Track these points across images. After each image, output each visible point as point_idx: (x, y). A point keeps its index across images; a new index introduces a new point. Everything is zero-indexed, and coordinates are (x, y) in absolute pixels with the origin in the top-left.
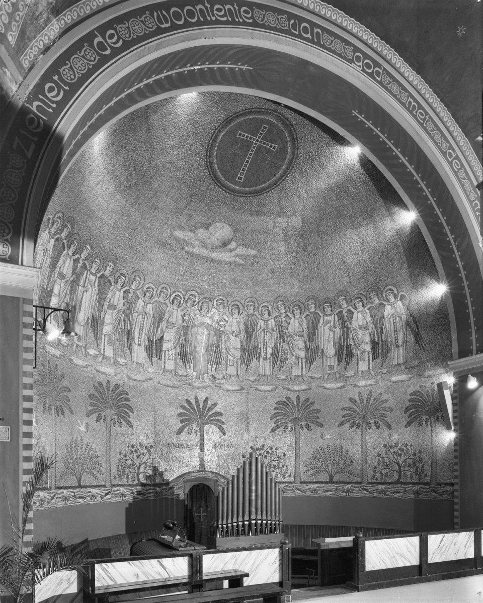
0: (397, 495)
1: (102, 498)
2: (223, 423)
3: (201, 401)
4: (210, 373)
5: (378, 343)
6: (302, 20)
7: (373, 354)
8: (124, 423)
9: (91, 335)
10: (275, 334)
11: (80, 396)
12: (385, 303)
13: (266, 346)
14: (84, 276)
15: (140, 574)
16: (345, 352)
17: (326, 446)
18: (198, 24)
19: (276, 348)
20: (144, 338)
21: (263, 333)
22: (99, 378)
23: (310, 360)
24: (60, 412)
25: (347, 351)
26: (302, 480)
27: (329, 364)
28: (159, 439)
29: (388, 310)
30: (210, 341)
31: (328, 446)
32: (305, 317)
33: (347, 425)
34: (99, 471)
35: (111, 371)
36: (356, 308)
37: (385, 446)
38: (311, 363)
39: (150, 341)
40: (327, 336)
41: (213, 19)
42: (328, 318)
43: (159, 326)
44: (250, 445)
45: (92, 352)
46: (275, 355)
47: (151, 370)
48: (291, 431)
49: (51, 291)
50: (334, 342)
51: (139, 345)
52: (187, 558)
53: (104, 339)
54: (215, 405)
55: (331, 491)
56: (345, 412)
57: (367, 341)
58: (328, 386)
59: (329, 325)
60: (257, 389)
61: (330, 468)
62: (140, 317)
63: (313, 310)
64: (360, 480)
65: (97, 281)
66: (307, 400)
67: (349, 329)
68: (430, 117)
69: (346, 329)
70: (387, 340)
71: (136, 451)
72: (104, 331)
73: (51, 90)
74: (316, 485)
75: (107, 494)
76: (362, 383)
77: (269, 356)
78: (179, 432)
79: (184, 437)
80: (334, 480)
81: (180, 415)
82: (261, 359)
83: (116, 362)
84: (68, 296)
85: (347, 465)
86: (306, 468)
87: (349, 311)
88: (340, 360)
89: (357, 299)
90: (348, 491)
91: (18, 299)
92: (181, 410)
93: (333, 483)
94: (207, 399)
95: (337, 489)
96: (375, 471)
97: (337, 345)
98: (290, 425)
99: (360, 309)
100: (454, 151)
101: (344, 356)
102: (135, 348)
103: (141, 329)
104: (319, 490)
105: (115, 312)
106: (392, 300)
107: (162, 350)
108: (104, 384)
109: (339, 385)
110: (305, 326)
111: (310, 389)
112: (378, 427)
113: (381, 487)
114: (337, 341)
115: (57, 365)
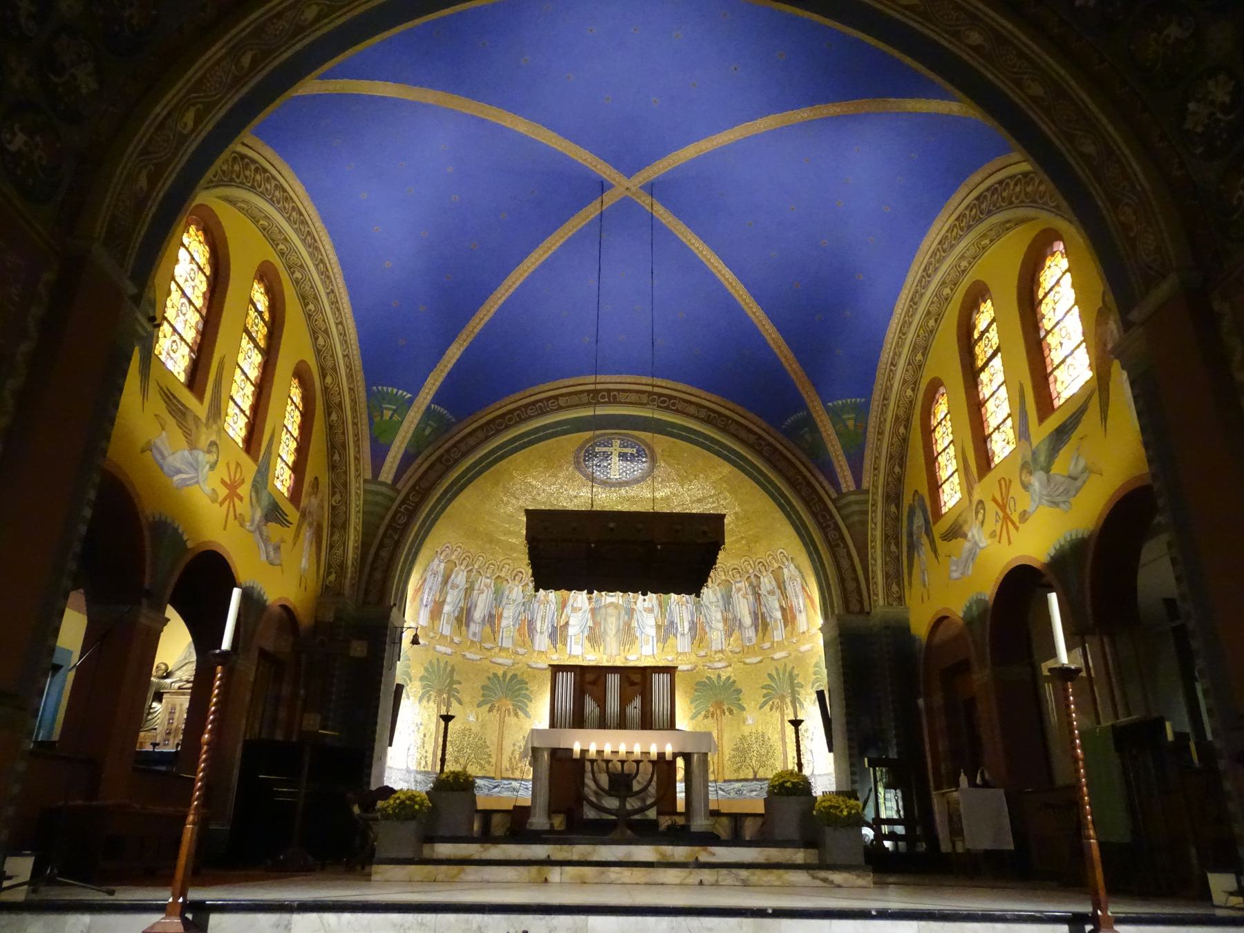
1: (489, 790)
9: (488, 629)
14: (479, 582)
19: (693, 621)
26: (726, 778)
32: (718, 585)
34: (489, 763)
38: (731, 635)
46: (693, 627)
50: (750, 613)
51: (542, 633)
55: (756, 791)
56: (765, 691)
58: (748, 661)
59: (741, 592)
62: (542, 606)
66: (729, 678)
67: (759, 595)
75: (495, 787)
77: (686, 632)
80: (758, 777)
82: (678, 635)
88: (757, 631)
102: (537, 637)
103: (543, 618)
108: (500, 673)
109: (758, 659)
110: (719, 596)
111: (730, 666)
114: (752, 610)
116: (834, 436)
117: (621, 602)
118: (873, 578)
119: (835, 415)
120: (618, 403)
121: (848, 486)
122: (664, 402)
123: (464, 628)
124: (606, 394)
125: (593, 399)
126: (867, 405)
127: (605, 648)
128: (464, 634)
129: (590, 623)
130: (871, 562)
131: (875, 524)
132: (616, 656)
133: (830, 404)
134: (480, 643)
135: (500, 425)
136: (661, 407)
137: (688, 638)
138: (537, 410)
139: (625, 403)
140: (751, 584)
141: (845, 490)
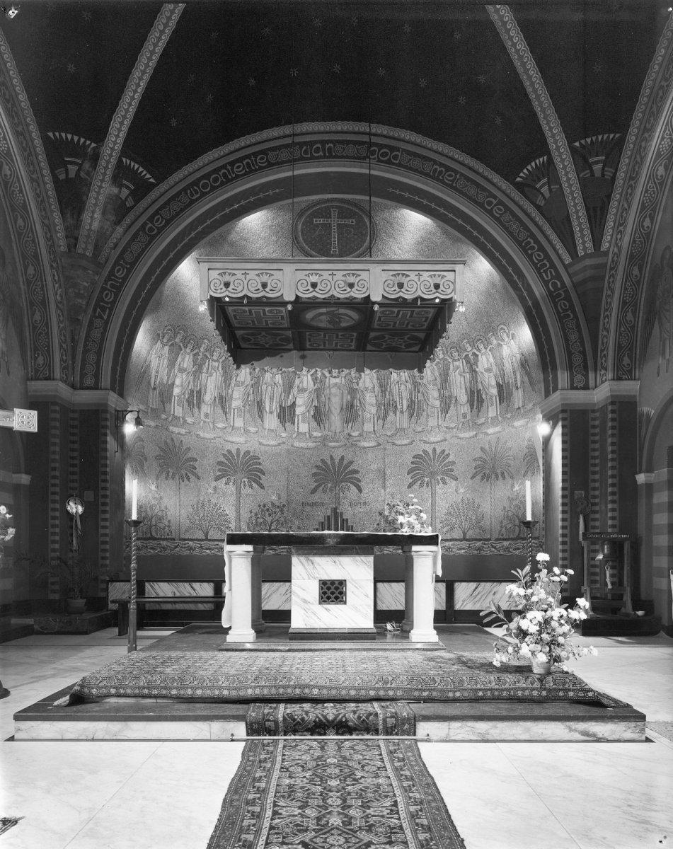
0: (517, 552)
2: (360, 481)
3: (337, 461)
4: (346, 432)
5: (502, 386)
6: (312, 143)
7: (500, 398)
8: (254, 485)
9: (219, 411)
10: (409, 385)
11: (207, 465)
12: (502, 343)
13: (401, 398)
15: (176, 592)
16: (476, 398)
17: (460, 500)
18: (223, 184)
19: (411, 400)
20: (275, 405)
21: (397, 386)
22: (228, 447)
23: (445, 410)
24: (185, 479)
25: (478, 397)
27: (462, 412)
28: (292, 498)
29: (506, 351)
30: (345, 401)
31: (462, 500)
32: (436, 365)
33: (479, 477)
35: (242, 440)
36: (479, 350)
37: (509, 498)
39: (282, 408)
40: (458, 381)
41: (234, 176)
42: (457, 363)
43: (289, 393)
44: (387, 502)
45: (221, 425)
47: (284, 435)
48: (428, 486)
49: (173, 384)
50: (466, 391)
52: (212, 584)
53: (234, 413)
54: (351, 463)
55: (464, 549)
57: (493, 384)
58: (461, 435)
60: (394, 444)
61: (463, 524)
63: (441, 356)
64: (489, 537)
65: (220, 366)
66: (443, 451)
68: (462, 174)
69: (473, 372)
70: (508, 382)
71: (268, 510)
72: (233, 406)
73: (118, 271)
74: (451, 543)
76: (491, 431)
77: (405, 408)
78: (313, 492)
79: (316, 497)
80: (468, 537)
81: (314, 474)
82: (398, 413)
83: (247, 432)
84: (191, 383)
85: (480, 519)
86: (441, 525)
87: (474, 354)
88: (472, 406)
89: (478, 340)
90: (479, 549)
91: (98, 410)
92: (315, 470)
93: (466, 540)
94: (343, 457)
95: (469, 547)
96: (501, 527)
97: (468, 390)
98: (426, 479)
99: (483, 351)
100: (495, 197)
101: (476, 402)
102: (267, 417)
103: (271, 399)
104: (454, 548)
105: (242, 389)
106: (506, 339)
107: (294, 414)
108: (234, 452)
110: (437, 374)
111: (446, 440)
112: (504, 478)
113: (506, 544)
115: (182, 441)
116: (576, 188)
117: (343, 382)
118: (602, 351)
119: (581, 158)
120: (334, 157)
121: (585, 249)
122: (384, 155)
123: (196, 410)
124: (319, 145)
125: (306, 153)
126: (620, 144)
127: (330, 426)
128: (196, 415)
129: (315, 403)
130: (602, 333)
131: (612, 291)
132: (340, 433)
133: (577, 144)
134: (213, 423)
135: (205, 186)
136: (382, 162)
137: (406, 415)
138: (244, 169)
139: (342, 157)
140: (468, 362)
141: (581, 253)
